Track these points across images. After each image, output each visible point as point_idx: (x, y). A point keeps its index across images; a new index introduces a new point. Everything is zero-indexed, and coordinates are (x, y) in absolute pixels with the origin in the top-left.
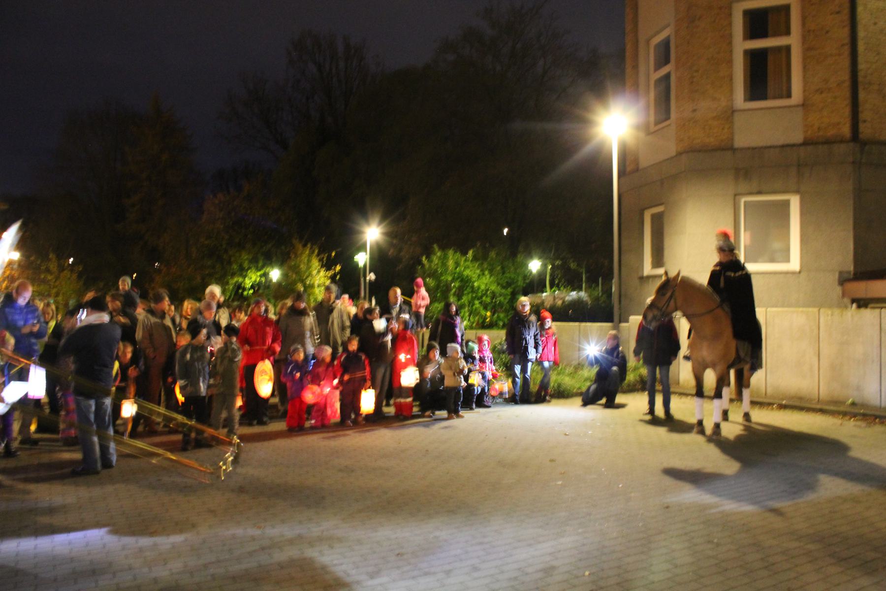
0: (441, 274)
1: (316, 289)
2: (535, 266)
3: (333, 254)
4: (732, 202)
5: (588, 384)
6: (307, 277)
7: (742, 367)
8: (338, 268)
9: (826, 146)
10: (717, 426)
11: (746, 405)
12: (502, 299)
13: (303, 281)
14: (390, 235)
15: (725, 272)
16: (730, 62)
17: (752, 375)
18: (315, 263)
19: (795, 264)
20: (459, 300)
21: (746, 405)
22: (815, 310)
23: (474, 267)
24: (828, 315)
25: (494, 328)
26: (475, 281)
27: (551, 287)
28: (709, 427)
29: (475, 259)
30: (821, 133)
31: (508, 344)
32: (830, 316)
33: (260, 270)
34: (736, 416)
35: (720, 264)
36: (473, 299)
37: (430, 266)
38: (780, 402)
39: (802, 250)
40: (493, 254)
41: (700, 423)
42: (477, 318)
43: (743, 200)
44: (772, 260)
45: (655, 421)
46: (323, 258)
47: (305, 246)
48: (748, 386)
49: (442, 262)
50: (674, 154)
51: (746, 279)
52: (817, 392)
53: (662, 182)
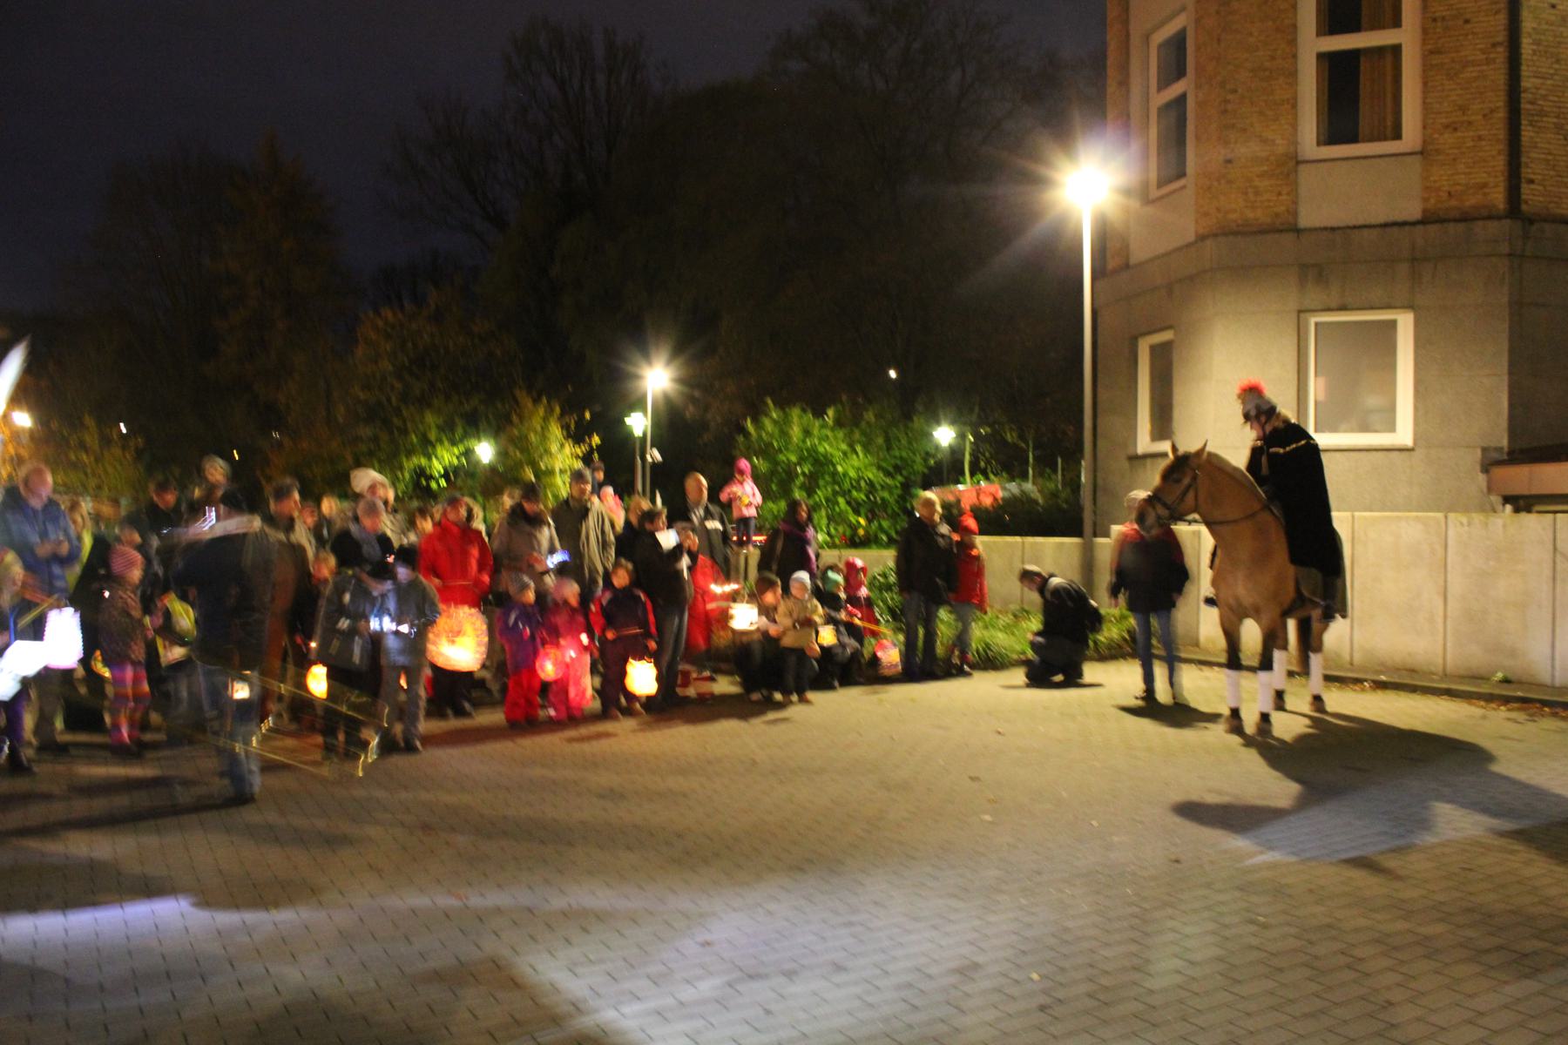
2: (944, 435)
8: (596, 440)
9: (1461, 227)
10: (1265, 718)
12: (886, 495)
15: (1269, 448)
17: (1325, 628)
18: (556, 431)
19: (1404, 434)
21: (1315, 683)
22: (1440, 515)
24: (1462, 524)
27: (972, 474)
28: (1250, 721)
29: (839, 423)
30: (1454, 203)
34: (1299, 701)
36: (835, 493)
37: (760, 436)
39: (1416, 409)
40: (870, 416)
41: (1235, 713)
42: (841, 529)
43: (1313, 320)
44: (1365, 428)
47: (536, 401)
48: (1319, 648)
50: (1191, 237)
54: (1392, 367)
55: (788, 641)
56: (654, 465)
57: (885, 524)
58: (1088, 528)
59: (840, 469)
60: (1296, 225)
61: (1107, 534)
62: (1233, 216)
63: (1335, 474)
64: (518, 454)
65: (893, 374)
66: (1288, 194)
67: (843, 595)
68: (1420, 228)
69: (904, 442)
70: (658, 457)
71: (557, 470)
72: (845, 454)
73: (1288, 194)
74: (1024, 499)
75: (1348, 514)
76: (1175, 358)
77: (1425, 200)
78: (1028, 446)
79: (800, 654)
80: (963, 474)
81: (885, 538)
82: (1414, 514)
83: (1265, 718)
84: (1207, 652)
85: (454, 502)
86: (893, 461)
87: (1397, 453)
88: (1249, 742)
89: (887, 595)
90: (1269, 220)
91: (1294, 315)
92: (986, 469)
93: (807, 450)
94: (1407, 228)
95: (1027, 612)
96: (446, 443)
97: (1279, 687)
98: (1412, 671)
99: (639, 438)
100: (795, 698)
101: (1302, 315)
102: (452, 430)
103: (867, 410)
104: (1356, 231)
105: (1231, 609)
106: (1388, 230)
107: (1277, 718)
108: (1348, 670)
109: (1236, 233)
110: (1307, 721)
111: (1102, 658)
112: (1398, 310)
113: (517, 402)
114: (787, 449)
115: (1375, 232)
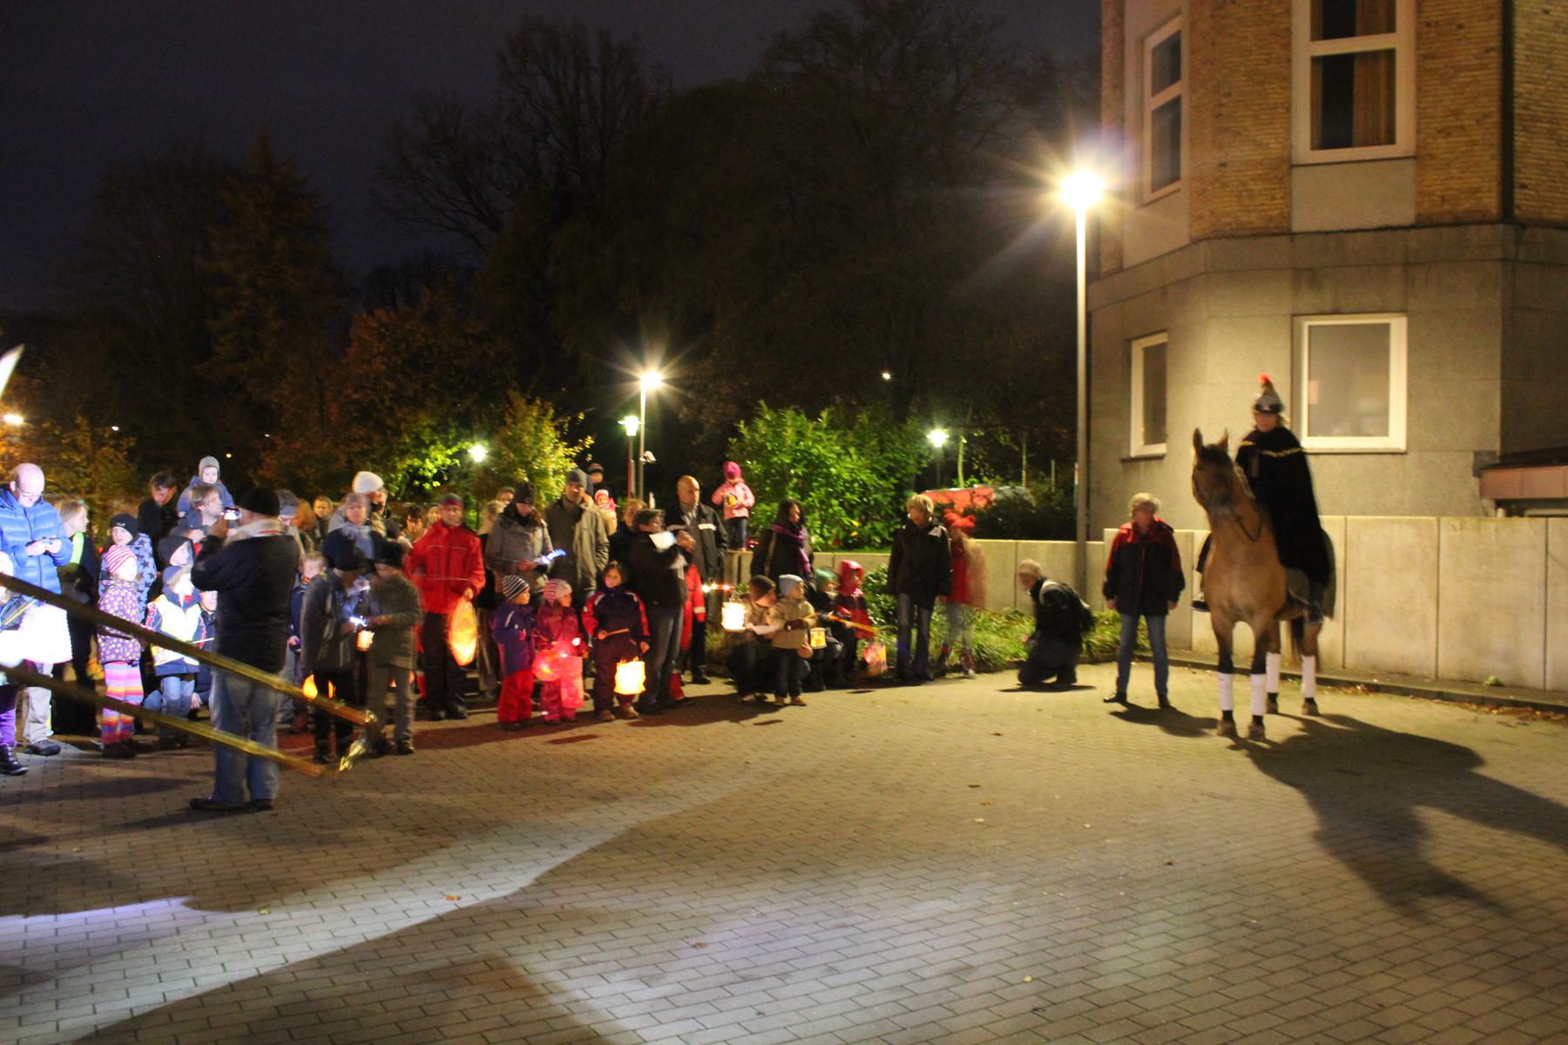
0: (773, 453)
2: (938, 438)
3: (581, 417)
6: (535, 458)
8: (590, 441)
9: (1454, 231)
10: (1258, 720)
12: (879, 496)
13: (526, 465)
16: (1286, 80)
18: (549, 433)
19: (1396, 438)
21: (1307, 687)
22: (1433, 519)
23: (829, 439)
24: (1454, 528)
26: (832, 466)
27: (966, 478)
28: (1243, 724)
29: (833, 425)
30: (1447, 207)
33: (449, 447)
34: (1292, 704)
36: (829, 495)
37: (753, 439)
38: (1368, 681)
39: (1409, 414)
40: (863, 418)
41: (1228, 715)
42: (834, 531)
43: (1307, 323)
44: (1357, 432)
45: (1135, 714)
47: (530, 402)
49: (774, 432)
50: (1186, 241)
51: (1300, 462)
53: (1163, 291)
54: (1385, 371)
55: (779, 643)
57: (879, 526)
59: (833, 470)
60: (1289, 228)
61: (1100, 538)
62: (1227, 220)
64: (512, 455)
65: (887, 376)
66: (1282, 198)
69: (898, 444)
70: (651, 457)
72: (839, 455)
75: (1342, 517)
77: (1418, 204)
79: (793, 655)
81: (878, 541)
82: (1407, 517)
83: (1258, 720)
84: (1200, 655)
86: (887, 463)
87: (1390, 456)
88: (1239, 744)
89: (881, 597)
91: (1288, 319)
92: (978, 471)
93: (800, 451)
94: (1400, 232)
95: (1021, 615)
96: (440, 446)
100: (788, 700)
101: (1295, 319)
103: (861, 412)
104: (1350, 235)
107: (1269, 720)
108: (1341, 673)
109: (1231, 237)
110: (1299, 724)
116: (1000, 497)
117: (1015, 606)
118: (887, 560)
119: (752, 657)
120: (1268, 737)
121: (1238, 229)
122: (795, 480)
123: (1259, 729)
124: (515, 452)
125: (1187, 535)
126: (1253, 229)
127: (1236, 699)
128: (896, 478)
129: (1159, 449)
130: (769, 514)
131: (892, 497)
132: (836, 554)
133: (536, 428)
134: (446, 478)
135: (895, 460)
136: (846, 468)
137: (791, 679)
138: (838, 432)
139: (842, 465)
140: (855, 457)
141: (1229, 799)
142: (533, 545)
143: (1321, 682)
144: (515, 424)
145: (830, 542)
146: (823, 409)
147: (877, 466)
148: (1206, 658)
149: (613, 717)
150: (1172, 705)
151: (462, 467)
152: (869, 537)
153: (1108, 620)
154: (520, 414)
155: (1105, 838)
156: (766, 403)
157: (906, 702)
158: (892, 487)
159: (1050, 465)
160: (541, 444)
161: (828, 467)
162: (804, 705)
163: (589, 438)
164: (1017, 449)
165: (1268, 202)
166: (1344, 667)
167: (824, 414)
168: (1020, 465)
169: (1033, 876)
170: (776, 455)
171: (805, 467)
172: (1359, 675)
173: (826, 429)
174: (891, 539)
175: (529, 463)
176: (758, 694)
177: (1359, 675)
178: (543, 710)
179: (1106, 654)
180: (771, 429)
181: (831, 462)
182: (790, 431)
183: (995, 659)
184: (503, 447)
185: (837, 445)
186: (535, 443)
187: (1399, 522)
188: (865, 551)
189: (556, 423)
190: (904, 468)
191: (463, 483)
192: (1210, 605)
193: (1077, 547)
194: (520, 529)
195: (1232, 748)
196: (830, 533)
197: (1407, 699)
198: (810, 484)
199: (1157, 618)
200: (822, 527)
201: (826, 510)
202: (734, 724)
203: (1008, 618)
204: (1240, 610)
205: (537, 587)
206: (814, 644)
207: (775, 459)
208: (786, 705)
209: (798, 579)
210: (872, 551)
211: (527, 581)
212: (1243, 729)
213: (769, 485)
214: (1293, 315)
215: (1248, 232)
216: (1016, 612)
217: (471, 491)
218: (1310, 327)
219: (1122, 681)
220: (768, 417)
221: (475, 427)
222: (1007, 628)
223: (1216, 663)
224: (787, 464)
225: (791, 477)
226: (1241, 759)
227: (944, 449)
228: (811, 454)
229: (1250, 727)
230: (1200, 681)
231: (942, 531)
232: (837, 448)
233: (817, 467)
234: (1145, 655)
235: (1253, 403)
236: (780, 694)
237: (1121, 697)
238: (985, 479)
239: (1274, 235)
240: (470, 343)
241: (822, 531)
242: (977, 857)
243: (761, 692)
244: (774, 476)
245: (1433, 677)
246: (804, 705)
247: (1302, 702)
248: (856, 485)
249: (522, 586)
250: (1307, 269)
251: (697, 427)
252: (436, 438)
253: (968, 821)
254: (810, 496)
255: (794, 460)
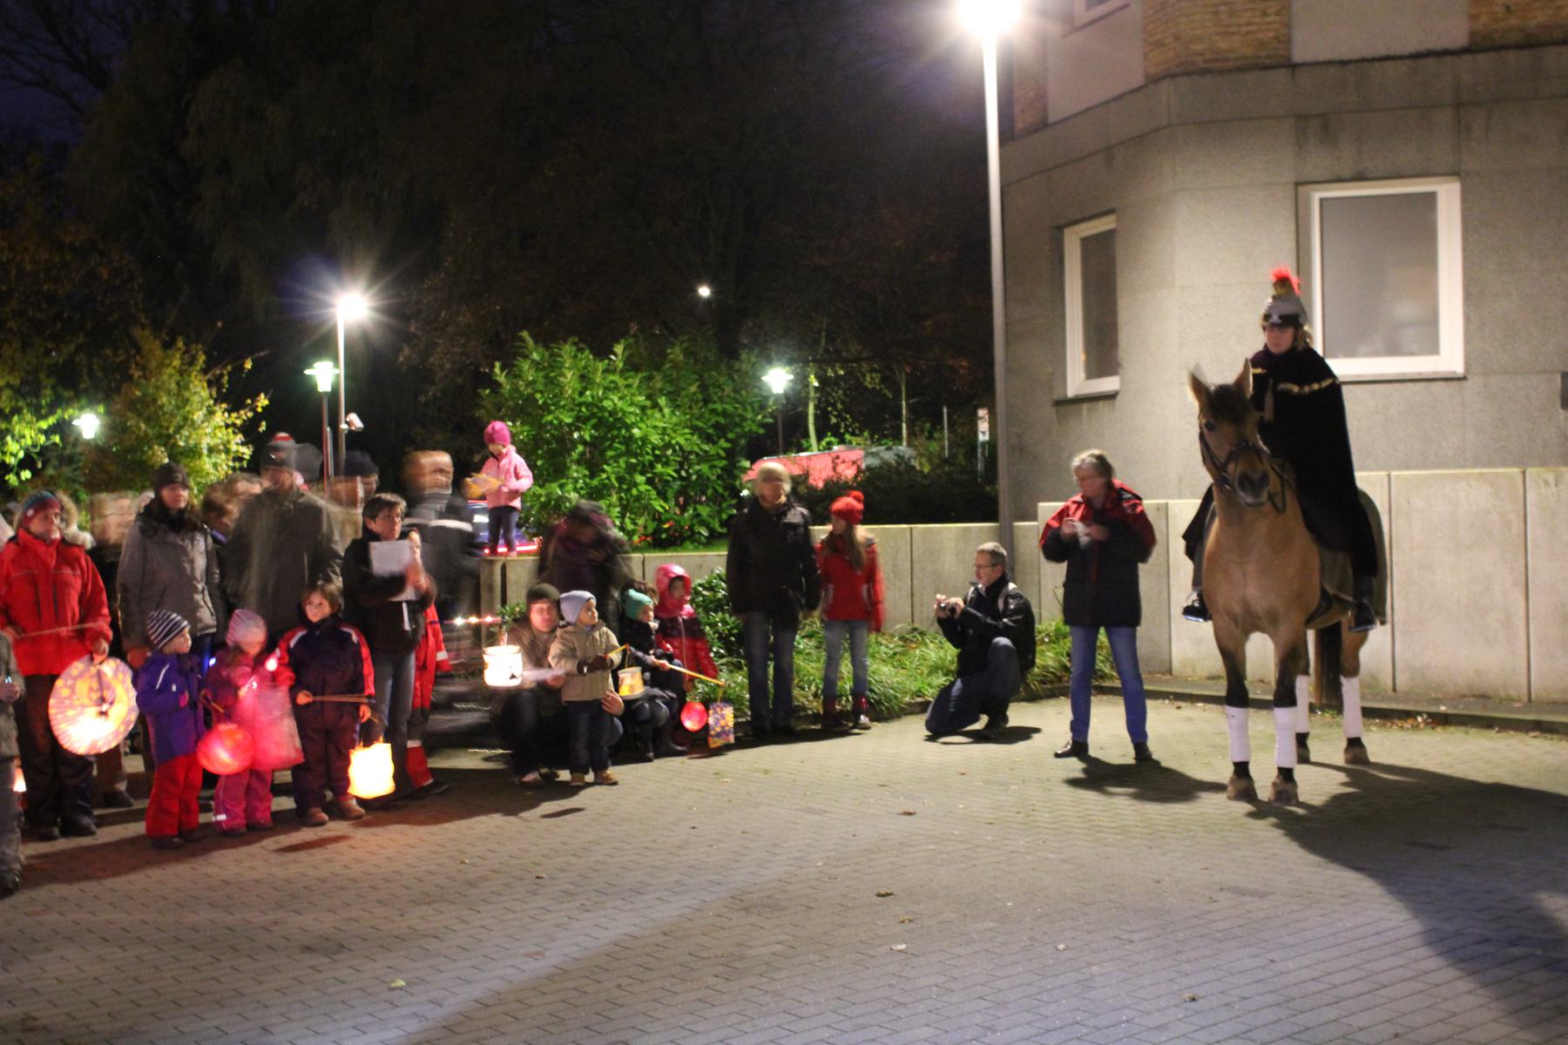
0: (545, 408)
1: (206, 459)
2: (778, 379)
3: (248, 365)
4: (1289, 203)
5: (941, 680)
6: (179, 429)
7: (1335, 621)
8: (263, 401)
9: (1525, 54)
10: (1286, 774)
11: (1351, 720)
12: (704, 468)
13: (167, 441)
14: (398, 313)
15: (1277, 382)
17: (1363, 639)
18: (200, 391)
19: (1451, 356)
20: (592, 476)
21: (1351, 720)
22: (1515, 471)
23: (629, 386)
24: (1546, 483)
25: (688, 544)
26: (634, 425)
27: (820, 438)
28: (1264, 781)
29: (632, 366)
30: (1513, 21)
31: (730, 589)
32: (1553, 485)
33: (44, 417)
34: (1329, 747)
35: (1262, 359)
36: (631, 469)
37: (515, 389)
38: (1433, 709)
39: (1467, 320)
40: (676, 353)
41: (1242, 769)
42: (641, 521)
43: (1317, 195)
44: (1394, 350)
45: (1099, 776)
46: (222, 376)
47: (168, 345)
48: (1354, 671)
49: (546, 377)
50: (1138, 80)
51: (1331, 398)
52: (1524, 681)
53: (1108, 153)
54: (1429, 260)
55: (571, 695)
56: (352, 435)
57: (704, 511)
58: (1004, 507)
59: (636, 431)
60: (1289, 59)
61: (1034, 517)
62: (1198, 47)
63: (1358, 413)
64: (143, 426)
65: (704, 291)
66: (1277, 14)
67: (654, 625)
68: (1468, 58)
69: (728, 390)
70: (356, 421)
71: (204, 446)
72: (643, 409)
73: (1277, 14)
74: (902, 468)
75: (1383, 473)
76: (1120, 255)
77: (1473, 18)
78: (897, 392)
79: (595, 708)
80: (807, 435)
81: (705, 533)
82: (1477, 471)
83: (1286, 774)
84: (1185, 681)
85: (42, 505)
86: (714, 419)
87: (1443, 383)
88: (1260, 811)
89: (718, 617)
90: (1249, 52)
91: (1290, 191)
92: (837, 426)
93: (588, 405)
94: (1449, 59)
95: (922, 634)
96: (28, 417)
97: (1301, 730)
98: (1484, 697)
99: (325, 393)
100: (590, 777)
101: (1301, 189)
102: (37, 394)
103: (672, 345)
104: (1377, 65)
105: (1234, 618)
106: (1422, 62)
107: (1301, 773)
108: (1391, 700)
109: (1204, 72)
110: (1342, 777)
111: (1033, 697)
112: (1441, 179)
113: (139, 350)
114: (557, 405)
115: (1403, 67)
116: (874, 462)
117: (913, 621)
118: (724, 561)
119: (529, 714)
120: (1301, 799)
121: (1216, 60)
122: (580, 448)
123: (1288, 787)
124: (148, 420)
125: (1158, 507)
126: (1237, 59)
127: (1253, 743)
128: (727, 440)
129: (1108, 384)
130: (543, 499)
131: (722, 468)
132: (647, 555)
133: (178, 384)
134: (40, 465)
135: (724, 414)
136: (655, 427)
137: (593, 745)
138: (640, 375)
139: (649, 423)
140: (667, 411)
141: (1263, 895)
142: (192, 562)
143: (1368, 713)
144: (145, 377)
145: (636, 538)
146: (618, 342)
147: (700, 424)
148: (1193, 684)
149: (325, 817)
150: (1155, 757)
151: (64, 448)
152: (691, 528)
153: (1048, 635)
154: (154, 364)
155: (1090, 965)
156: (532, 336)
157: (766, 772)
158: (722, 453)
159: (942, 413)
160: (188, 408)
161: (628, 427)
162: (615, 783)
163: (262, 396)
164: (890, 395)
165: (1257, 20)
166: (1394, 690)
167: (619, 349)
168: (898, 415)
169: (993, 1030)
170: (550, 412)
171: (595, 427)
172: (1417, 702)
173: (622, 372)
174: (724, 531)
175: (169, 437)
176: (544, 771)
177: (1417, 702)
178: (218, 812)
179: (1049, 686)
180: (542, 374)
181: (633, 419)
182: (569, 375)
183: (888, 699)
184: (130, 415)
185: (640, 394)
186: (178, 407)
187: (1467, 477)
188: (686, 549)
189: (209, 376)
190: (737, 425)
191: (67, 470)
192: (1211, 611)
193: (1000, 529)
194: (171, 537)
195: (1251, 815)
196: (635, 524)
197: (1492, 733)
198: (603, 452)
199: (1124, 631)
200: (623, 517)
201: (629, 490)
202: (511, 819)
203: (902, 638)
204: (1259, 618)
205: (200, 626)
206: (625, 691)
207: (550, 418)
208: (589, 785)
209: (587, 594)
210: (696, 549)
211: (185, 617)
212: (1264, 791)
213: (542, 457)
214: (1297, 184)
215: (1230, 64)
216: (915, 630)
217: (80, 483)
218: (1322, 201)
219: (1080, 725)
220: (535, 356)
221: (82, 386)
222: (903, 654)
223: (1223, 693)
224: (569, 425)
225: (574, 444)
226: (1266, 830)
227: (786, 396)
228: (602, 409)
229: (1274, 784)
230: (1190, 719)
231: (802, 514)
232: (641, 399)
233: (611, 427)
234: (1107, 684)
235: (1262, 311)
236: (579, 770)
237: (1079, 748)
238: (848, 437)
239: (1266, 68)
240: (68, 258)
241: (622, 523)
242: (904, 1005)
243: (549, 766)
244: (549, 443)
245: (1525, 699)
246: (615, 783)
247: (1344, 744)
248: (669, 452)
249: (177, 624)
250: (1315, 116)
251: (422, 374)
252: (20, 404)
253: (885, 949)
254: (604, 471)
255: (578, 418)
